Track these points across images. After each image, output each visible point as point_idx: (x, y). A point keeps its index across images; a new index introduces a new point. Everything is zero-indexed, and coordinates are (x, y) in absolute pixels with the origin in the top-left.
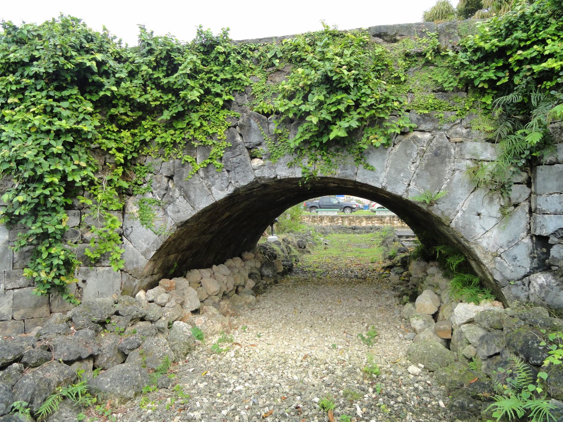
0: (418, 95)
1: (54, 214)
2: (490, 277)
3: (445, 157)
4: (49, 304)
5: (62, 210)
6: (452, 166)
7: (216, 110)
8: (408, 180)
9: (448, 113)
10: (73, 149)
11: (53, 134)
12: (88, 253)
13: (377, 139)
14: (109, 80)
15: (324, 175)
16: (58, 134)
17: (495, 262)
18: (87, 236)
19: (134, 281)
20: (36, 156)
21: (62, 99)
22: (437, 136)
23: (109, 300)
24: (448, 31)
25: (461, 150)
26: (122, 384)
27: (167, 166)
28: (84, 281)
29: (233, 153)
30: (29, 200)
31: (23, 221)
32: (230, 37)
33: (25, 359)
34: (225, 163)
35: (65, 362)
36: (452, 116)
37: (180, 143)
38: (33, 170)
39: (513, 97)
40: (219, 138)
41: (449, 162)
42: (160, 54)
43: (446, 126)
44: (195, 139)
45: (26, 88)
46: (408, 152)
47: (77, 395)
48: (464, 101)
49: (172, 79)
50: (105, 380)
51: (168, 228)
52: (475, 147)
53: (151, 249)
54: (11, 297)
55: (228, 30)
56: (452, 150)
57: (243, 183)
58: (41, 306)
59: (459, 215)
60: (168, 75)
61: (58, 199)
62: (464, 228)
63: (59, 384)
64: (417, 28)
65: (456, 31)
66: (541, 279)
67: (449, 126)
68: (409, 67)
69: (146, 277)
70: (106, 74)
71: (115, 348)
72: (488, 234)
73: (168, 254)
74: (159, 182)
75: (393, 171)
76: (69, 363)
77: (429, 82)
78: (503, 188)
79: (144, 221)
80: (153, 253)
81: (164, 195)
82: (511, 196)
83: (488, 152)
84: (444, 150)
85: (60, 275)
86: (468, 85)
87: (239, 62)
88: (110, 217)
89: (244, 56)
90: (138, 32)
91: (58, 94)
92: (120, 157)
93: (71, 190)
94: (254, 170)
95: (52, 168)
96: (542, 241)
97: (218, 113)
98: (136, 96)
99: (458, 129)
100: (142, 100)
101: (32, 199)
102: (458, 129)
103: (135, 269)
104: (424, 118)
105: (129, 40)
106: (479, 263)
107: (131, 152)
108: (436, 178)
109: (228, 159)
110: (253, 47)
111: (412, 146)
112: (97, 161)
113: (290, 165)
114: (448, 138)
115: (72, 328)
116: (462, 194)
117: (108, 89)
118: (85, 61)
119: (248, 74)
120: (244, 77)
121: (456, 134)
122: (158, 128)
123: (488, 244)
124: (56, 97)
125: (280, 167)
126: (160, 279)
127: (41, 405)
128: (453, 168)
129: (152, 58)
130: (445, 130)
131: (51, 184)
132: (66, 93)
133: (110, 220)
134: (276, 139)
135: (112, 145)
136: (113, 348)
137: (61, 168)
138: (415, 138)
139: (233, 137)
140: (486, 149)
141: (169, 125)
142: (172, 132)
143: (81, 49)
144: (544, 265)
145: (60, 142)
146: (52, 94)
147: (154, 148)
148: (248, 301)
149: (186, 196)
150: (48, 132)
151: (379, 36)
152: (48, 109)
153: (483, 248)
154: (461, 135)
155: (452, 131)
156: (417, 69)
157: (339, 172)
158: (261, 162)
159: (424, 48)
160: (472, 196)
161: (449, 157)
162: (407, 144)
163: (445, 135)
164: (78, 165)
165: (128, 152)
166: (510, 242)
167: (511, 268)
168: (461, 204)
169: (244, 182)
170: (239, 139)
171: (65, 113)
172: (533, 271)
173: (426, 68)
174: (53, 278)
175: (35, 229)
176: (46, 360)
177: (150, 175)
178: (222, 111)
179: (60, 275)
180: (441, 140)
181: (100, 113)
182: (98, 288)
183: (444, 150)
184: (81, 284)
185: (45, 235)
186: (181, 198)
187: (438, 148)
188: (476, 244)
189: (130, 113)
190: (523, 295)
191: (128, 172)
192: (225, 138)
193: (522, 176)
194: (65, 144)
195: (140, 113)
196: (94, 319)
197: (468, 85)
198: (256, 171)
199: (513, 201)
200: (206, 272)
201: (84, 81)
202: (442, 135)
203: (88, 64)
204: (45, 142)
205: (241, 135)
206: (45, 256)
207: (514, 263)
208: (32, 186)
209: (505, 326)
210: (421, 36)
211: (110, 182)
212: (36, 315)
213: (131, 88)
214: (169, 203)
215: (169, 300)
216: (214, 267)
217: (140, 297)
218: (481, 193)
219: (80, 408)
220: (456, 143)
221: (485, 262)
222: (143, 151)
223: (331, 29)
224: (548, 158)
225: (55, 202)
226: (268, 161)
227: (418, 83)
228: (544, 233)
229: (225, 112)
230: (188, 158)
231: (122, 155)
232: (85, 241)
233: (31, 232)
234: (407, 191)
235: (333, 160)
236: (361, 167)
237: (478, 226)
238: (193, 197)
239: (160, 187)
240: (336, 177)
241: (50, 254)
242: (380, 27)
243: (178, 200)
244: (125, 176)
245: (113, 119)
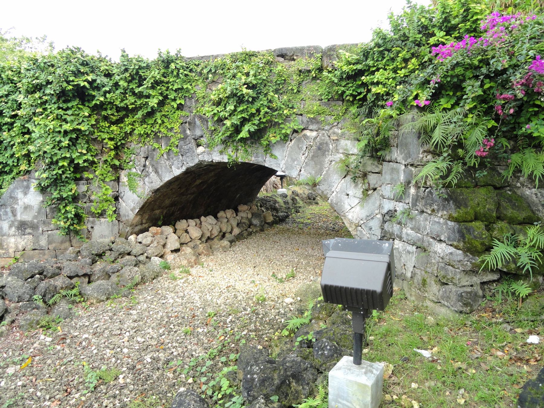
1: (67, 185)
3: (325, 151)
4: (70, 241)
5: (73, 182)
6: (329, 158)
7: (173, 111)
8: (300, 167)
9: (328, 117)
10: (78, 142)
11: (62, 134)
12: (93, 209)
13: (274, 137)
14: (99, 92)
15: (243, 161)
16: (66, 133)
17: (357, 231)
18: (93, 197)
19: (127, 228)
20: (52, 148)
21: (67, 109)
22: (320, 135)
23: (107, 240)
24: (329, 53)
25: (337, 146)
26: (98, 292)
27: (143, 150)
28: (92, 227)
29: (185, 143)
30: (50, 176)
31: (49, 189)
32: (183, 54)
33: (45, 273)
34: (180, 149)
35: (68, 277)
36: (331, 119)
37: (150, 134)
38: (51, 158)
40: (175, 131)
41: (328, 155)
42: (133, 71)
43: (327, 128)
44: (160, 132)
45: (46, 101)
46: (300, 146)
47: (71, 295)
49: (140, 89)
50: (89, 289)
51: (146, 193)
52: (346, 145)
53: (136, 207)
54: (47, 236)
55: (180, 50)
56: (331, 146)
57: (192, 165)
58: (65, 242)
59: (334, 194)
60: (139, 87)
61: (68, 176)
62: (337, 204)
63: (62, 288)
64: (308, 50)
65: (335, 53)
67: (329, 127)
68: (303, 81)
69: (136, 226)
70: (98, 88)
71: (104, 271)
72: (353, 209)
73: (153, 210)
74: (139, 161)
75: (289, 160)
76: (71, 278)
79: (132, 188)
80: (137, 210)
81: (143, 170)
82: (371, 182)
84: (325, 145)
85: (74, 223)
86: (341, 97)
87: (186, 75)
88: (105, 186)
89: (191, 71)
90: (120, 53)
91: (65, 106)
92: (111, 144)
93: (77, 169)
94: (198, 155)
95: (63, 156)
97: (175, 112)
98: (117, 103)
99: (336, 130)
100: (122, 105)
101: (52, 175)
102: (336, 130)
103: (127, 220)
104: (313, 121)
105: (116, 58)
107: (120, 140)
108: (319, 166)
109: (181, 146)
110: (197, 63)
111: (303, 141)
112: (96, 147)
113: (221, 153)
114: (329, 136)
115: (79, 257)
116: (336, 179)
117: (98, 100)
118: (80, 82)
119: (193, 84)
120: (190, 87)
121: (334, 133)
122: (137, 123)
123: (353, 217)
124: (64, 108)
126: (150, 227)
127: (51, 298)
128: (331, 159)
129: (127, 75)
130: (326, 130)
131: (63, 166)
132: (70, 105)
133: (104, 188)
134: (212, 133)
135: (105, 136)
136: (102, 271)
137: (68, 155)
138: (305, 136)
139: (185, 131)
141: (143, 121)
142: (145, 126)
143: (77, 73)
145: (67, 138)
146: (61, 106)
147: (135, 137)
148: (223, 245)
149: (157, 172)
150: (60, 132)
151: (282, 56)
152: (59, 117)
153: (349, 220)
154: (337, 134)
155: (331, 131)
156: (308, 82)
157: (253, 159)
159: (311, 67)
160: (343, 181)
161: (328, 151)
162: (299, 140)
163: (326, 134)
164: (81, 153)
165: (118, 140)
166: (368, 216)
167: (368, 235)
168: (335, 187)
169: (192, 163)
170: (188, 132)
171: (69, 119)
173: (314, 81)
174: (69, 226)
175: (55, 195)
176: (57, 275)
177: (134, 155)
178: (177, 112)
179: (74, 223)
180: (323, 138)
181: (96, 114)
182: (102, 232)
183: (325, 145)
184: (90, 229)
185: (61, 199)
186: (153, 173)
187: (321, 144)
188: (345, 216)
189: (116, 114)
191: (119, 153)
192: (179, 131)
193: (378, 167)
194: (70, 140)
195: (124, 113)
196: (93, 252)
198: (200, 156)
199: (372, 186)
200: (192, 222)
201: (82, 95)
202: (324, 134)
203: (82, 84)
204: (58, 139)
206: (63, 211)
207: (370, 232)
208: (53, 167)
211: (106, 161)
212: (62, 247)
213: (115, 97)
214: (146, 176)
215: (152, 242)
216: (203, 218)
217: (131, 239)
219: (74, 303)
220: (333, 140)
222: (128, 139)
223: (248, 50)
225: (66, 177)
227: (308, 93)
229: (179, 112)
230: (156, 145)
231: (113, 142)
232: (91, 201)
233: (53, 197)
234: (299, 175)
235: (249, 150)
237: (347, 204)
238: (160, 173)
239: (140, 164)
240: (251, 162)
241: (66, 210)
242: (282, 49)
243: (151, 175)
244: (117, 156)
245: (106, 118)
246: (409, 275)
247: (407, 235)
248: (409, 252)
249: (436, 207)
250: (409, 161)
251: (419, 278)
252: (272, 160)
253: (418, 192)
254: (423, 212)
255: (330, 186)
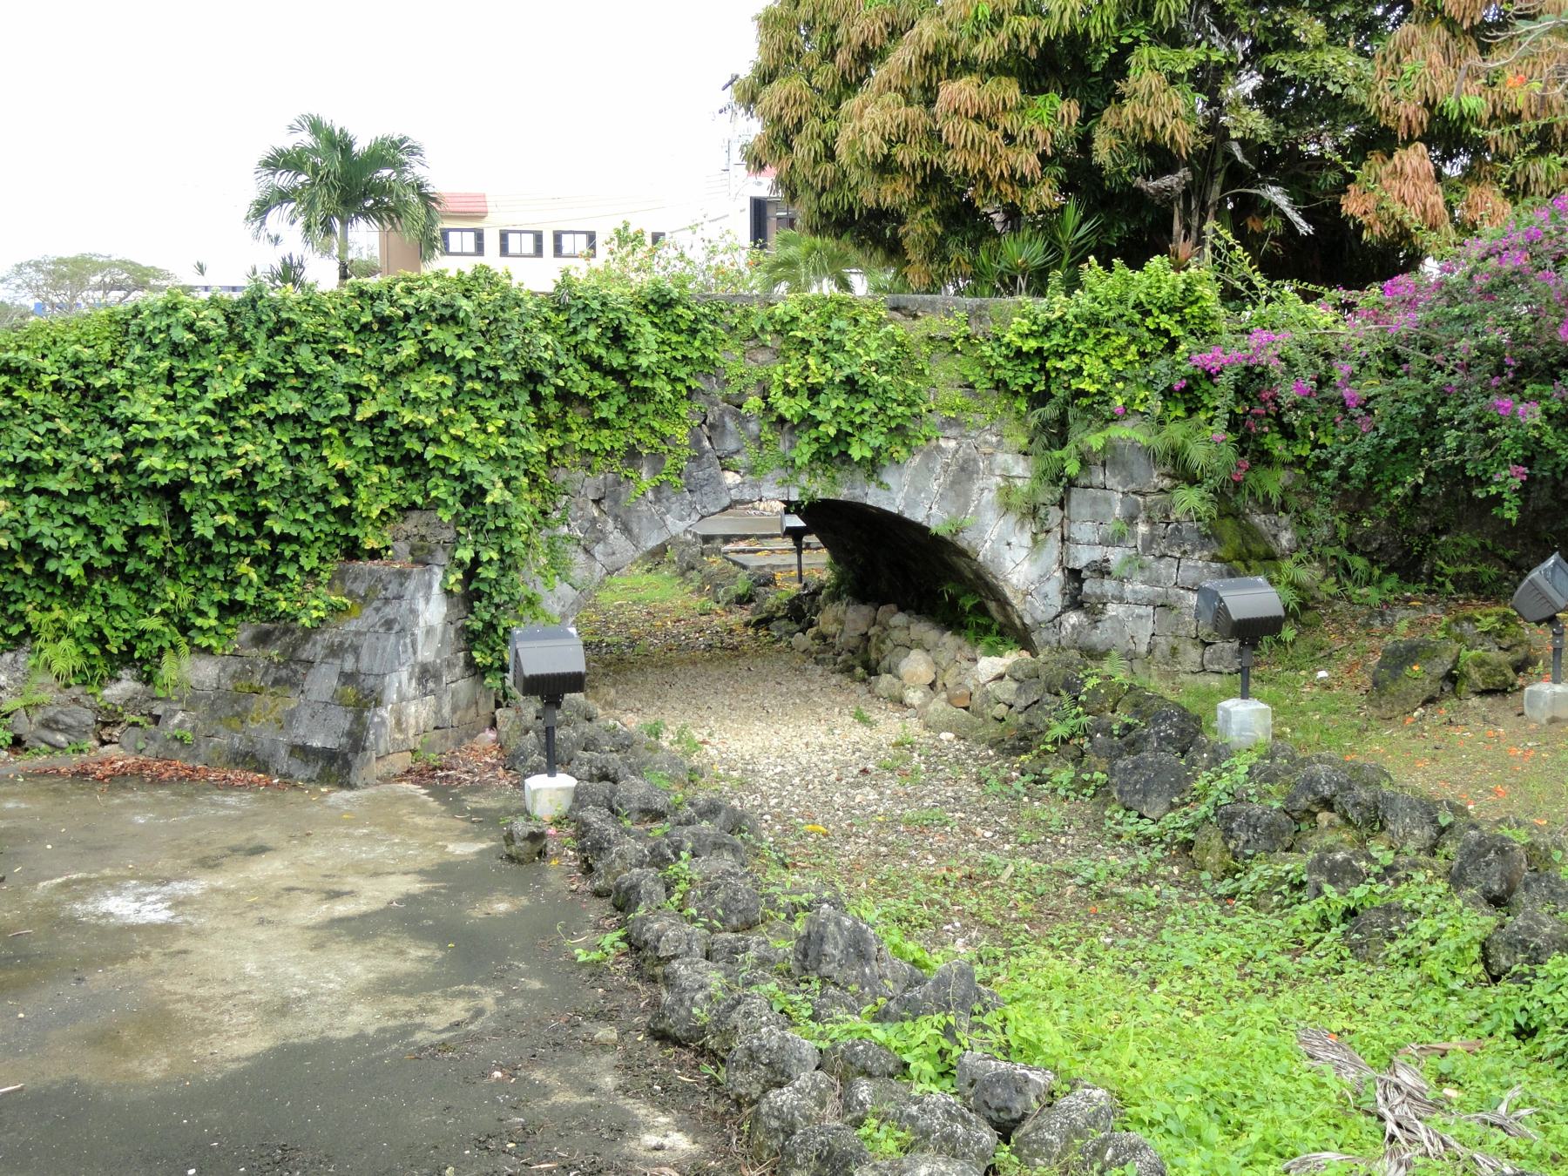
0: (942, 390)
2: (1017, 621)
6: (980, 484)
39: (1050, 411)
48: (997, 402)
66: (1073, 618)
77: (954, 375)
78: (1033, 512)
83: (1020, 468)
86: (1000, 385)
96: (1075, 575)
104: (949, 422)
106: (1003, 603)
125: (766, 486)
140: (1017, 463)
144: (1075, 602)
149: (626, 529)
157: (845, 491)
158: (738, 479)
159: (953, 334)
170: (707, 444)
172: (1065, 609)
186: (616, 533)
187: (965, 461)
190: (1053, 640)
197: (1000, 385)
205: (709, 438)
209: (1041, 673)
210: (947, 316)
218: (1012, 518)
221: (1014, 602)
224: (1082, 482)
226: (748, 477)
228: (1077, 566)
234: (928, 516)
235: (838, 476)
236: (873, 484)
237: (1007, 557)
246: (1143, 649)
247: (1135, 592)
248: (1140, 617)
249: (1188, 547)
250: (1133, 486)
251: (1163, 644)
252: (879, 491)
253: (1152, 530)
254: (1163, 556)
255: (982, 532)
